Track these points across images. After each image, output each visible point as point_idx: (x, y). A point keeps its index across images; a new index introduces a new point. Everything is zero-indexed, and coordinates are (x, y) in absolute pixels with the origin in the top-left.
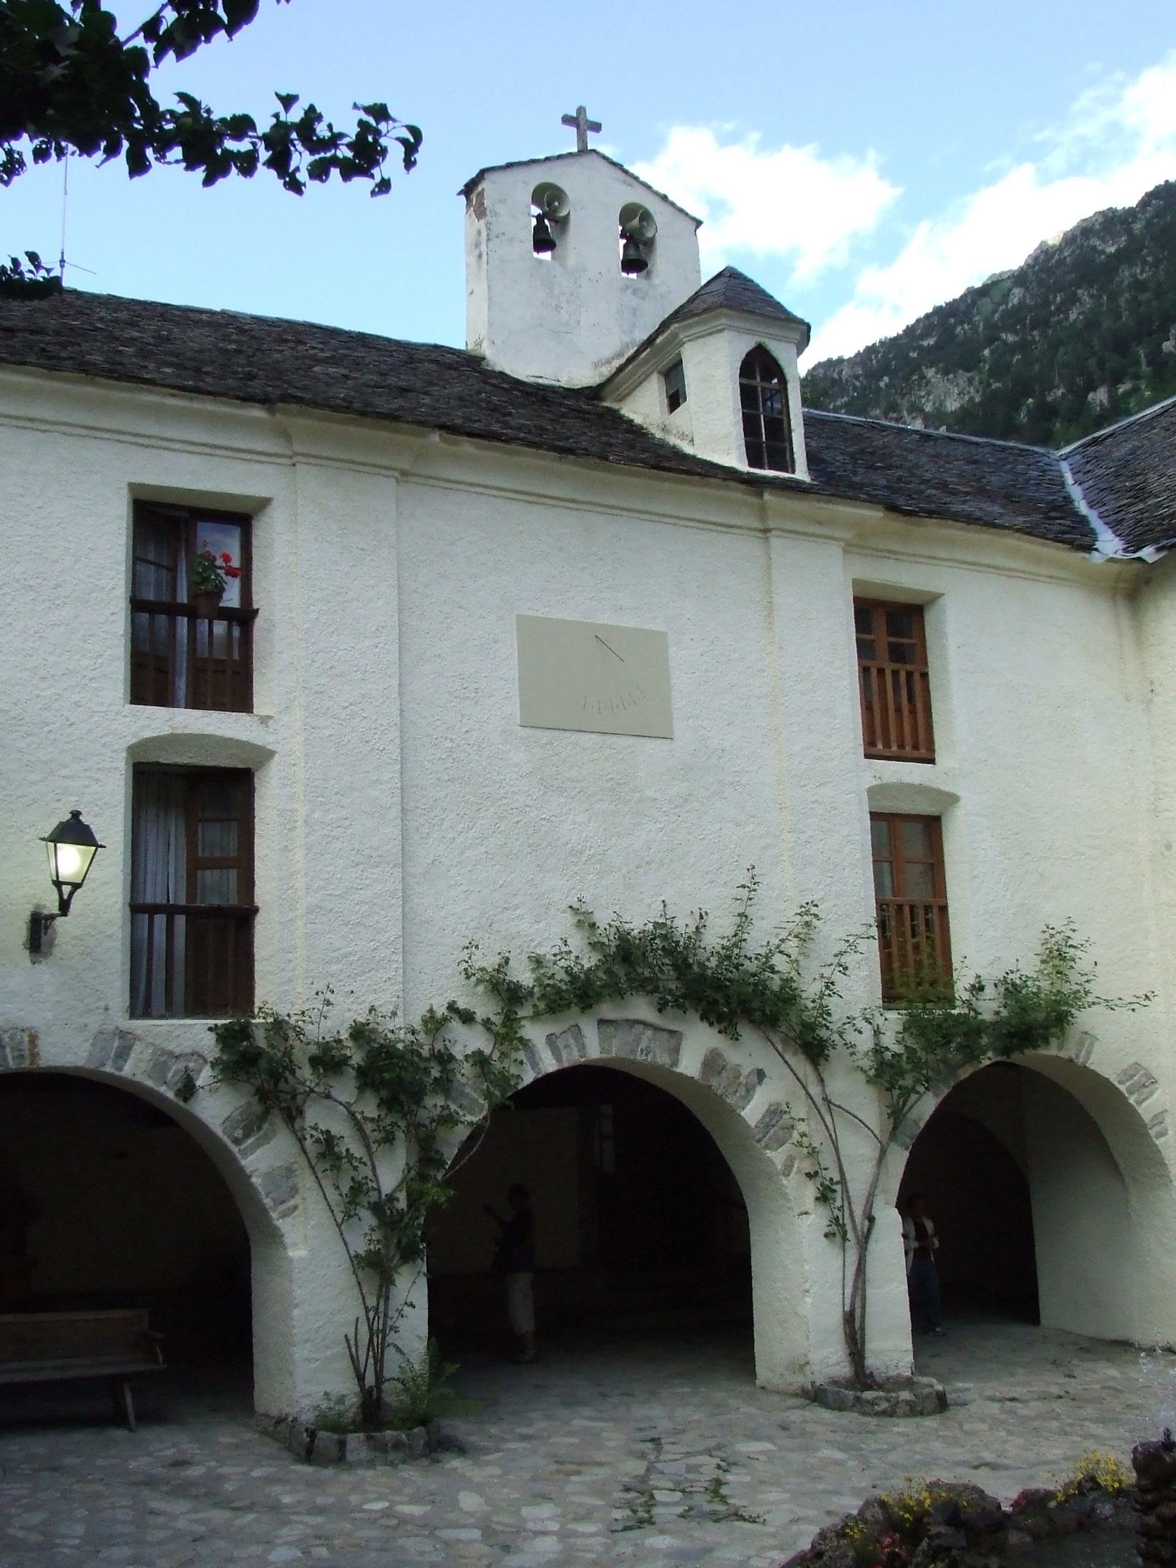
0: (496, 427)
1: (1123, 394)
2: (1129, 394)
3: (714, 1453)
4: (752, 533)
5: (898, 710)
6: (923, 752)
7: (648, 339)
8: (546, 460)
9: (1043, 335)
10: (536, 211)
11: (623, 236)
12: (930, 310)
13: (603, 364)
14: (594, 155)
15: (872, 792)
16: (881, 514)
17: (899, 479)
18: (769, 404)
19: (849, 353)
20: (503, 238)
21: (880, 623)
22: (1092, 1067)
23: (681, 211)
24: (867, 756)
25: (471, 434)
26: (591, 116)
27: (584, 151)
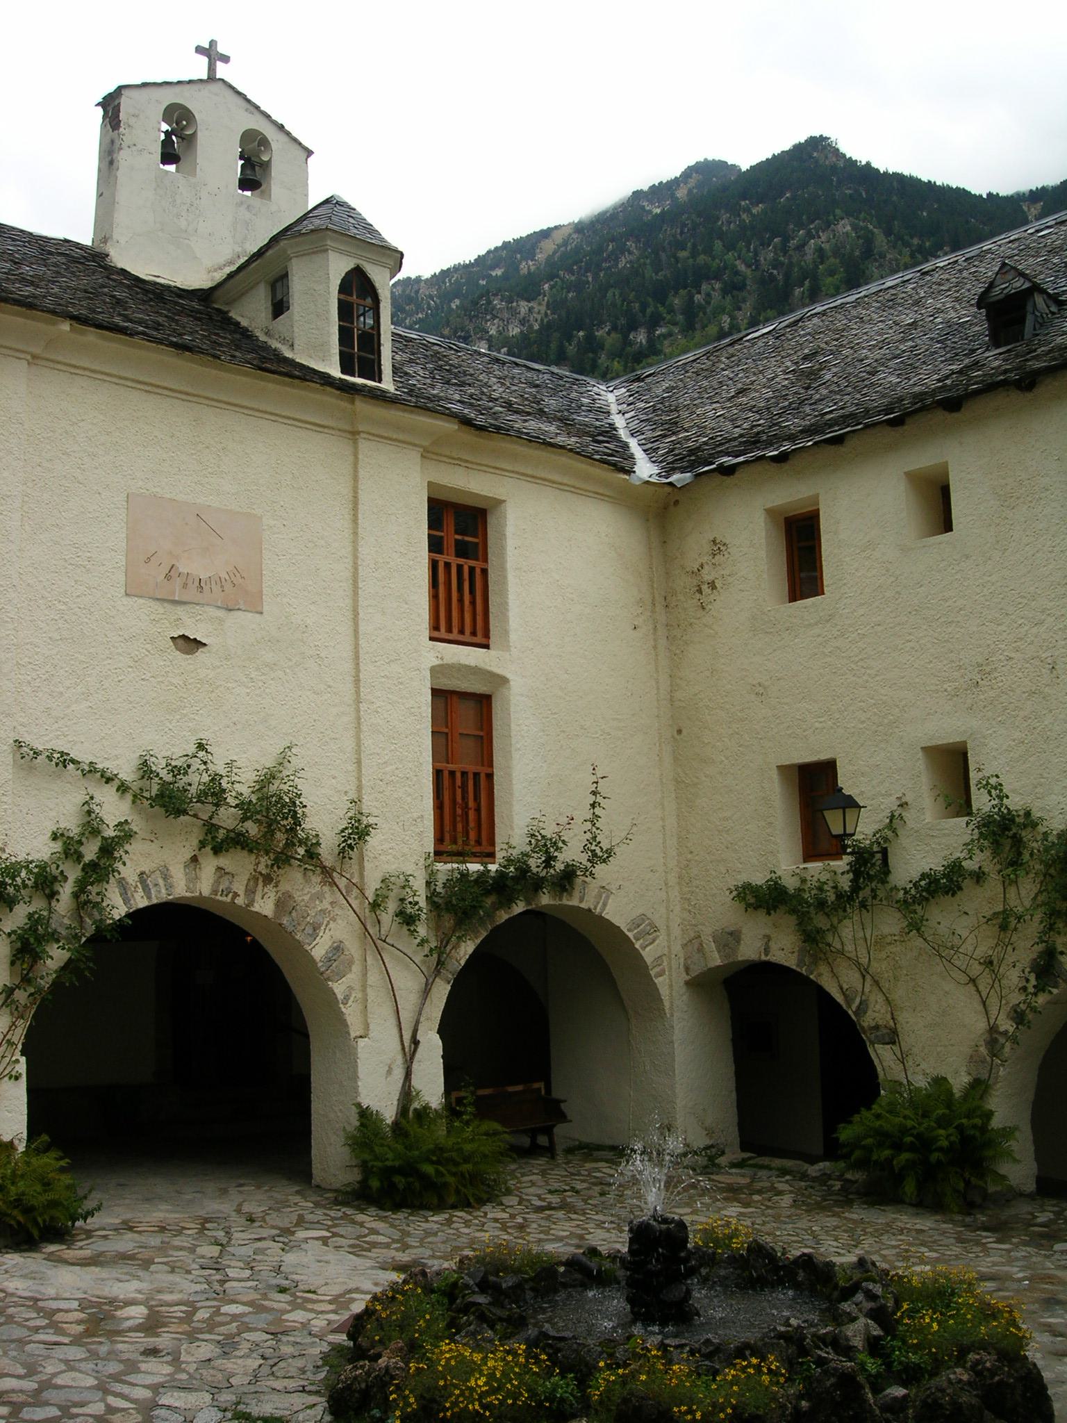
0: (117, 320)
1: (659, 336)
2: (665, 336)
3: (277, 1239)
4: (344, 435)
5: (461, 600)
6: (479, 639)
7: (259, 250)
8: (167, 357)
9: (596, 277)
10: (165, 127)
11: (241, 158)
12: (500, 244)
13: (215, 270)
14: (221, 82)
15: (434, 670)
16: (456, 427)
17: (471, 396)
18: (362, 319)
19: (426, 274)
20: (134, 148)
21: (449, 523)
22: (607, 917)
23: (295, 140)
24: (431, 639)
25: (99, 326)
26: (221, 49)
27: (212, 78)
